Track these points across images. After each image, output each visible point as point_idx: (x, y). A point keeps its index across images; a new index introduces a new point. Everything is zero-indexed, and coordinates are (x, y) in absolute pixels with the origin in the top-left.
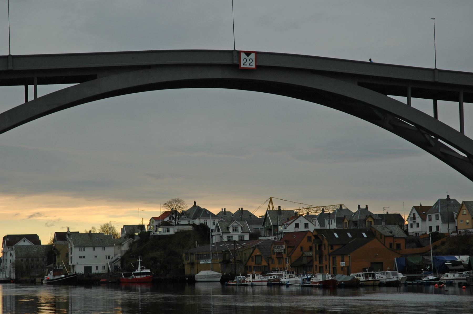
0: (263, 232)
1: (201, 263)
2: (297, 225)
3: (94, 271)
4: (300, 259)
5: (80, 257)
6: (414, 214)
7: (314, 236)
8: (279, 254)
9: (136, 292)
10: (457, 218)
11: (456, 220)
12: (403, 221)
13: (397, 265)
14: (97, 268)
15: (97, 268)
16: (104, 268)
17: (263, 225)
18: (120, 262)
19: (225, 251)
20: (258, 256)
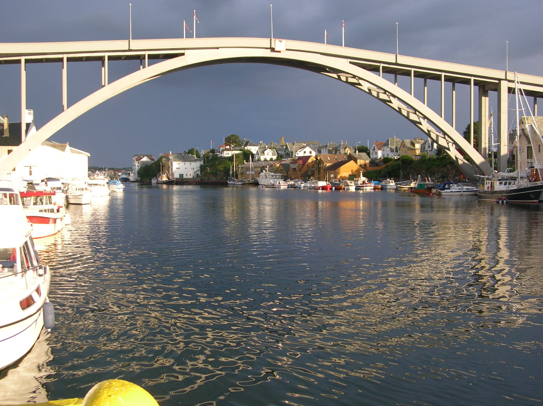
0: (284, 156)
1: (248, 173)
2: (305, 152)
3: (185, 177)
4: (307, 172)
5: (8, 174)
6: (374, 147)
7: (48, 141)
8: (295, 169)
9: (441, 148)
10: (399, 150)
11: (399, 151)
12: (189, 361)
13: (169, 373)
14: (187, 175)
15: (187, 175)
16: (190, 175)
17: (285, 152)
18: (200, 172)
19: (262, 167)
20: (282, 170)
